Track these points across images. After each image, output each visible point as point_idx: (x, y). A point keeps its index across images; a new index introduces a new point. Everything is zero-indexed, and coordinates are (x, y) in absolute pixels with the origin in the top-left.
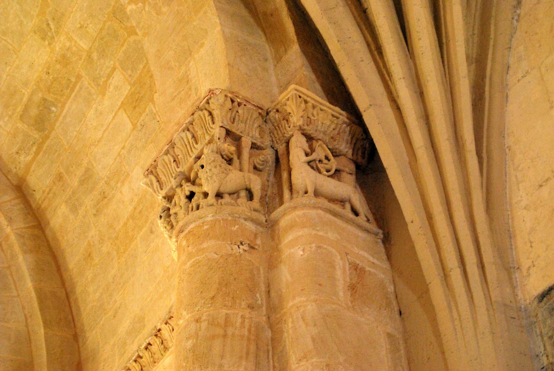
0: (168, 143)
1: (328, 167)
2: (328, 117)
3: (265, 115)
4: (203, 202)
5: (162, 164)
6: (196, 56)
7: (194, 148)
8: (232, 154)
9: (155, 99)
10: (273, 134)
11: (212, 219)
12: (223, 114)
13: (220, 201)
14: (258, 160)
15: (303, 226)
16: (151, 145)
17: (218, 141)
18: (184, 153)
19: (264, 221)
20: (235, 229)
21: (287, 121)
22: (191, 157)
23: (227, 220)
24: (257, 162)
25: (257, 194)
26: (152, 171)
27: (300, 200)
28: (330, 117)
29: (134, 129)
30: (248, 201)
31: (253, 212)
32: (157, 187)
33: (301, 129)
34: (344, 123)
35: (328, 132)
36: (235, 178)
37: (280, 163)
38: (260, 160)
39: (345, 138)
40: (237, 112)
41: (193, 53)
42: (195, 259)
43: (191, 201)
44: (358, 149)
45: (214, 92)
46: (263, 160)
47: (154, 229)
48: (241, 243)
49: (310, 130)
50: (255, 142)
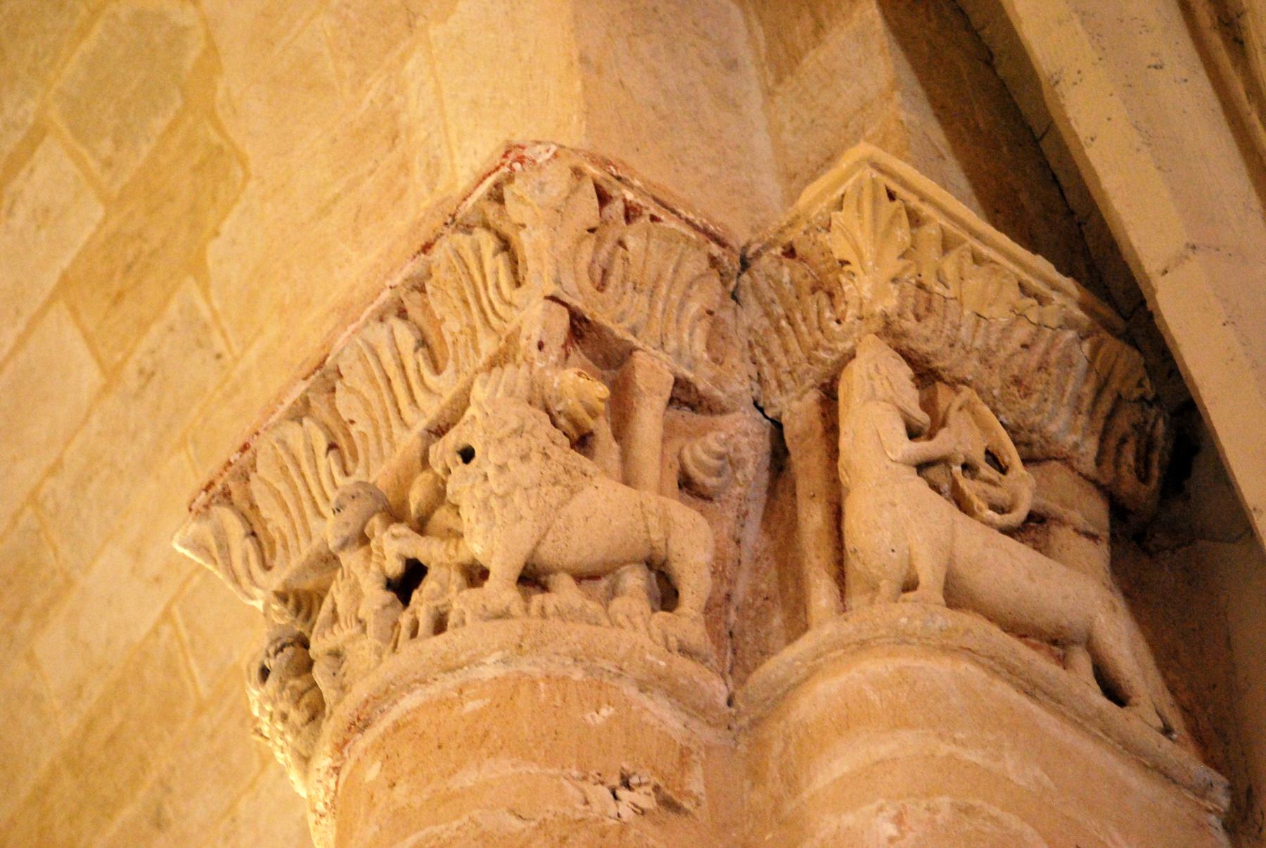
1: (998, 494)
2: (1004, 295)
3: (734, 267)
6: (435, 31)
7: (428, 390)
8: (593, 413)
9: (210, 262)
10: (766, 352)
11: (501, 672)
12: (563, 245)
13: (537, 599)
14: (700, 452)
15: (899, 721)
16: (183, 456)
17: (535, 352)
18: (378, 414)
19: (722, 700)
20: (599, 719)
21: (831, 295)
22: (405, 425)
23: (565, 679)
25: (695, 587)
26: (228, 491)
27: (880, 613)
28: (1012, 293)
29: (106, 389)
30: (654, 611)
31: (679, 659)
32: (246, 560)
33: (889, 331)
34: (1068, 323)
35: (1002, 354)
36: (604, 510)
37: (791, 475)
38: (708, 451)
39: (1069, 389)
40: (621, 243)
41: (420, 22)
42: (422, 834)
43: (405, 599)
44: (1123, 441)
45: (527, 153)
46: (722, 449)
47: (169, 812)
48: (626, 784)
49: (925, 337)
50: (690, 375)
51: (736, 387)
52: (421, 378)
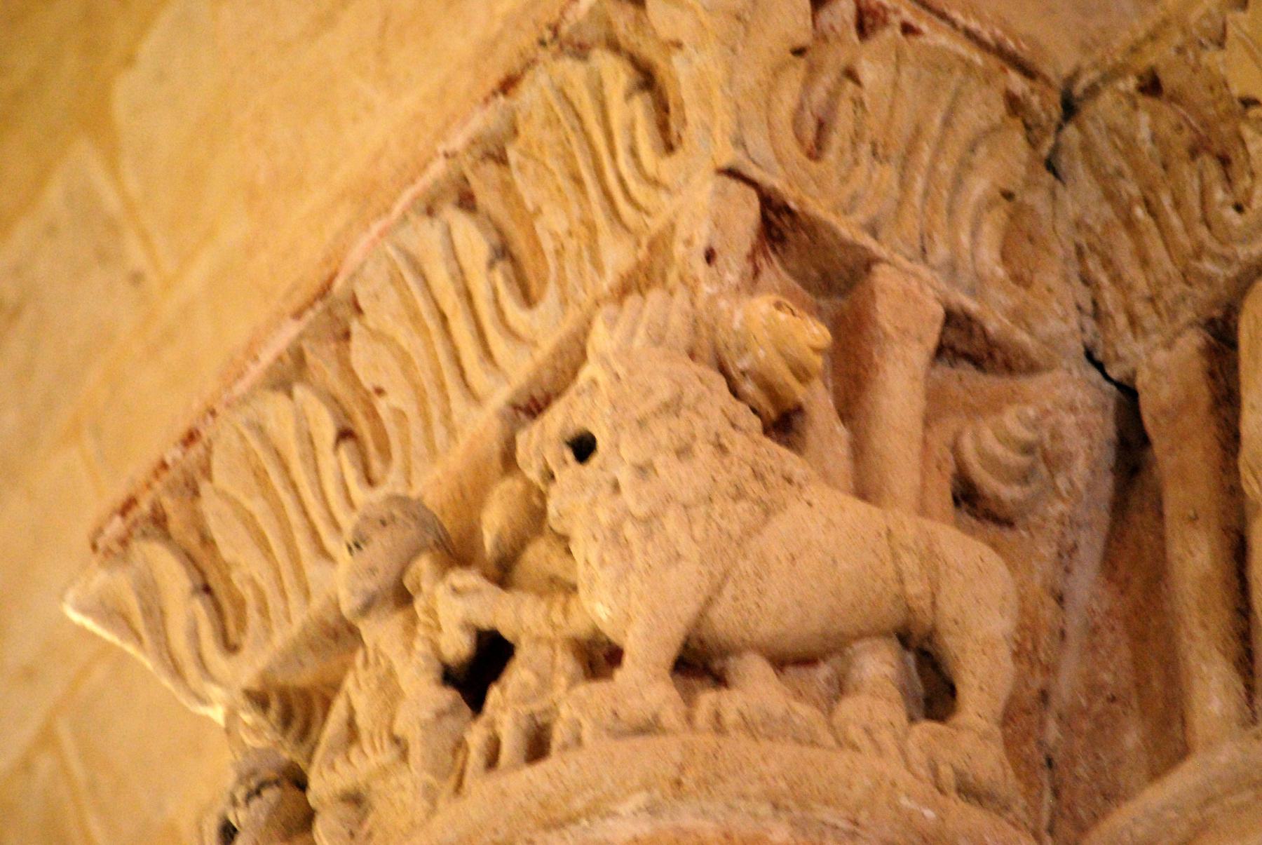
0: (299, 299)
4: (582, 706)
5: (248, 454)
7: (511, 333)
8: (802, 374)
11: (644, 828)
13: (707, 699)
14: (990, 442)
18: (425, 377)
21: (1224, 161)
24: (982, 454)
25: (984, 678)
30: (912, 719)
32: (194, 635)
36: (823, 542)
38: (1006, 439)
40: (851, 74)
50: (972, 306)
51: (1054, 326)
52: (500, 313)
